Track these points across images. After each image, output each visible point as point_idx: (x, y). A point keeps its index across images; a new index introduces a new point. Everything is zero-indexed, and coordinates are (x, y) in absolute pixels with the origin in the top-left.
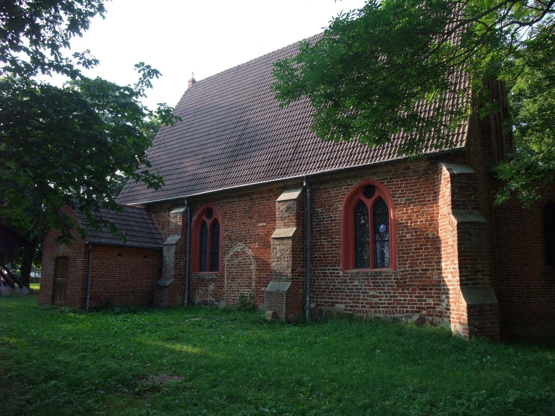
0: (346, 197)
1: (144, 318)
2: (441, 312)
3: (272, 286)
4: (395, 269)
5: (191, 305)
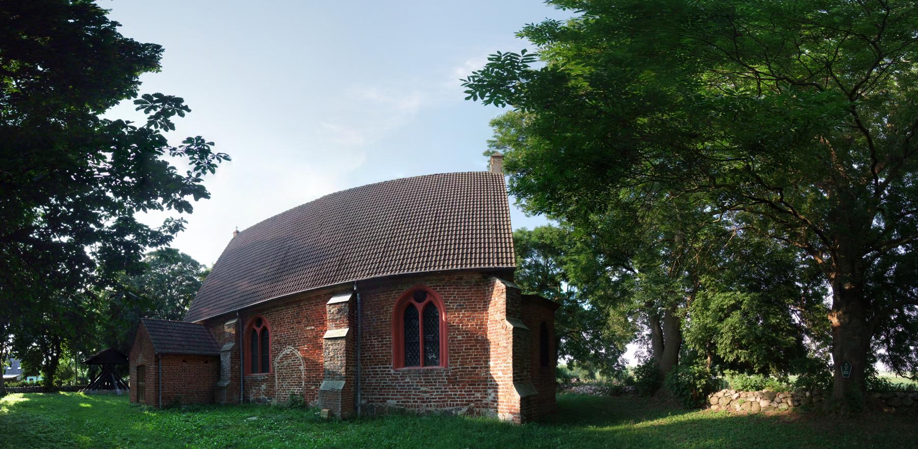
0: (397, 300)
1: (202, 418)
2: (487, 404)
3: (324, 385)
4: (446, 367)
5: (247, 404)
